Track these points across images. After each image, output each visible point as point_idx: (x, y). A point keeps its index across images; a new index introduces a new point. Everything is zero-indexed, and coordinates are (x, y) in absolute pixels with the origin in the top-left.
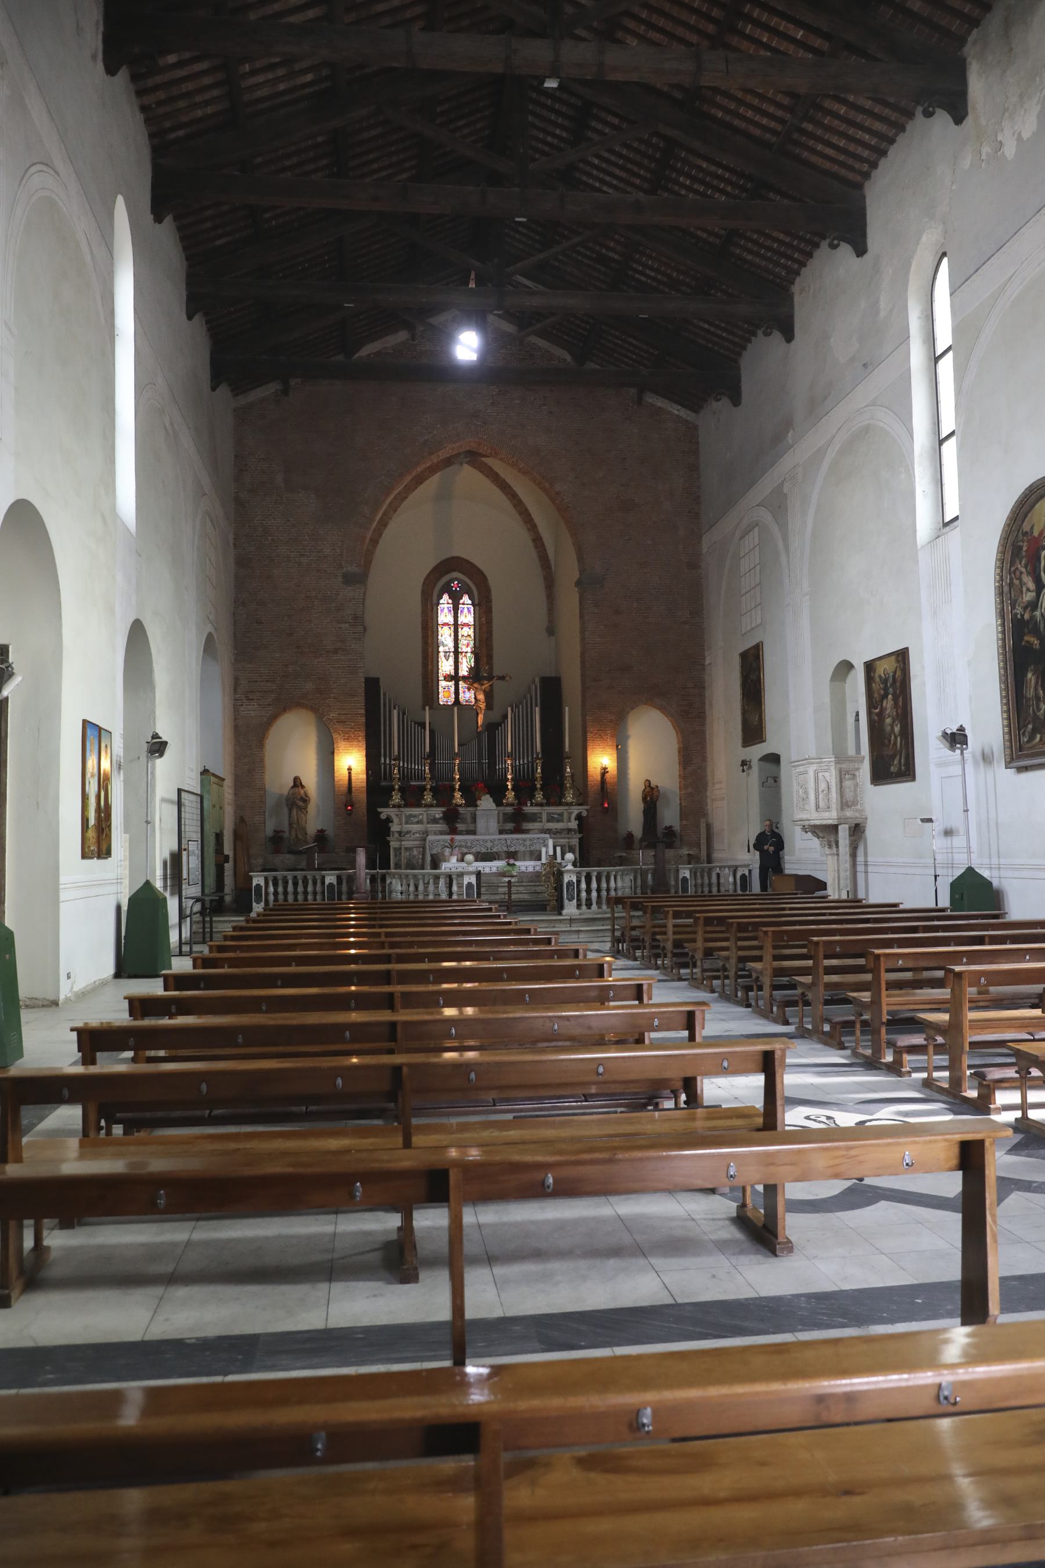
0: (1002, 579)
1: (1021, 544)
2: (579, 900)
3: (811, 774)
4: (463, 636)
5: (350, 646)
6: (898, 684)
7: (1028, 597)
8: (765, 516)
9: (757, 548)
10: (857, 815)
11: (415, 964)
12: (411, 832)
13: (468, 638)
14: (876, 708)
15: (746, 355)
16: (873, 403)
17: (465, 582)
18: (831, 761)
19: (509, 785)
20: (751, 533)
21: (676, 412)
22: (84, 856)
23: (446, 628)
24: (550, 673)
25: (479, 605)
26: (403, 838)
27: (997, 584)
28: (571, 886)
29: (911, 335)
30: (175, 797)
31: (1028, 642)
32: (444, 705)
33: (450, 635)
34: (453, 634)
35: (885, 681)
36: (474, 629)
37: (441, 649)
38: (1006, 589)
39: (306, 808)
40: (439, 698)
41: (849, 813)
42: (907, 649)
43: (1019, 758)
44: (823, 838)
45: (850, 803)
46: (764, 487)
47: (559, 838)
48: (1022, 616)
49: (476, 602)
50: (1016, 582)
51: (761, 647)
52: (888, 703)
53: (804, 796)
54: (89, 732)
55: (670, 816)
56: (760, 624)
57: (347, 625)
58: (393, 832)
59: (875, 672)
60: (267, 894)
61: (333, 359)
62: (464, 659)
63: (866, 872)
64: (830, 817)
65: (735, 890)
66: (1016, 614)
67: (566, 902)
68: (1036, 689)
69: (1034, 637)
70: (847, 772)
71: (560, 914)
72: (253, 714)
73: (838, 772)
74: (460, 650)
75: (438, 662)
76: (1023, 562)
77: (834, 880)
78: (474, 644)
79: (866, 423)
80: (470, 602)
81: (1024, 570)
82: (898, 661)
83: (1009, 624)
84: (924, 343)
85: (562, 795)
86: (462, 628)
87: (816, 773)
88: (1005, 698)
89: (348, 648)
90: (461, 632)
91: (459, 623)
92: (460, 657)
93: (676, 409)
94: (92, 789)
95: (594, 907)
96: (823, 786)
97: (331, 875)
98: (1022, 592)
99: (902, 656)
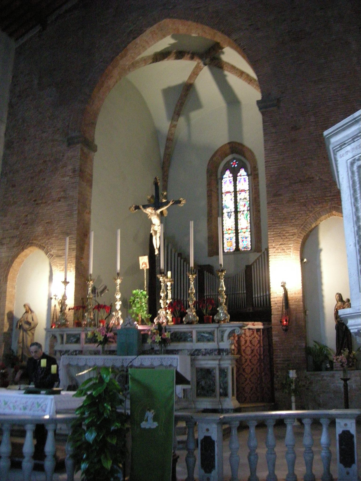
5: (69, 194)
13: (245, 200)
19: (223, 299)
23: (228, 195)
32: (227, 252)
33: (231, 200)
34: (233, 198)
37: (225, 211)
49: (250, 173)
53: (229, 239)
57: (68, 178)
62: (242, 216)
74: (238, 210)
78: (249, 204)
80: (245, 174)
85: (215, 312)
86: (240, 194)
89: (67, 196)
90: (239, 196)
91: (238, 190)
92: (239, 215)
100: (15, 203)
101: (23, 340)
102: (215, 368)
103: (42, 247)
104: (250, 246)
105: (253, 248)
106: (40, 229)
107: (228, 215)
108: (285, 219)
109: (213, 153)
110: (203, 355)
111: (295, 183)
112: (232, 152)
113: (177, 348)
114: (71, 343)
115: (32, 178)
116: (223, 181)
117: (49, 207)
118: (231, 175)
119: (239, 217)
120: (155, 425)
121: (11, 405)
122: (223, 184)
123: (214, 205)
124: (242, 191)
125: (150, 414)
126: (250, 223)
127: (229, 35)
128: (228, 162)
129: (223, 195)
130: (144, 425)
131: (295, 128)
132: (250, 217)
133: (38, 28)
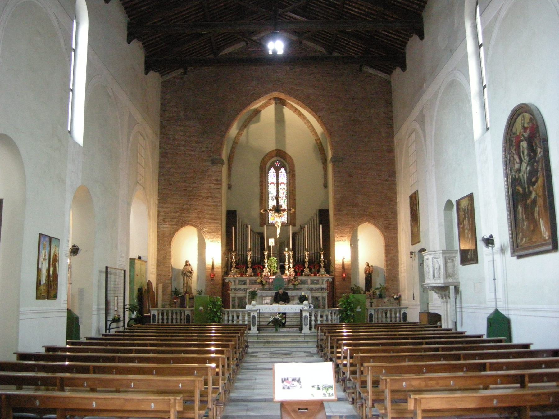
0: (506, 157)
1: (512, 139)
2: (310, 324)
3: (431, 260)
4: (281, 189)
5: (214, 195)
6: (469, 212)
7: (517, 166)
8: (417, 126)
9: (415, 143)
10: (455, 281)
11: (176, 355)
12: (240, 289)
13: (284, 190)
14: (461, 225)
15: (408, 46)
16: (455, 69)
17: (282, 162)
18: (440, 253)
19: (322, 265)
20: (412, 135)
21: (380, 75)
22: (38, 298)
23: (272, 185)
24: (323, 207)
25: (289, 173)
26: (237, 292)
27: (504, 160)
28: (306, 318)
29: (467, 35)
30: (104, 270)
31: (518, 190)
32: (271, 224)
33: (275, 188)
34: (276, 188)
35: (464, 211)
36: (287, 185)
37: (270, 196)
38: (508, 162)
39: (191, 276)
40: (268, 221)
41: (450, 280)
42: (472, 194)
43: (517, 251)
44: (439, 293)
45: (451, 275)
46: (416, 111)
47: (317, 293)
48: (515, 176)
49: (288, 172)
50: (512, 158)
51: (417, 193)
52: (466, 222)
54: (42, 240)
55: (378, 282)
56: (417, 181)
57: (213, 185)
58: (231, 289)
59: (460, 206)
60: (158, 319)
61: (208, 56)
62: (282, 200)
63: (462, 312)
64: (440, 282)
65: (400, 321)
66: (513, 175)
67: (304, 326)
68: (522, 215)
69: (520, 187)
70: (449, 258)
71: (301, 333)
72: (166, 229)
73: (444, 259)
74: (279, 196)
75: (268, 202)
76: (514, 148)
77: (444, 315)
78: (287, 193)
79: (452, 79)
80: (285, 172)
81: (514, 152)
82: (469, 200)
83: (510, 181)
84: (473, 39)
87: (433, 259)
88: (510, 219)
90: (280, 187)
91: (279, 182)
93: (380, 74)
94: (44, 266)
95: (313, 329)
96: (436, 266)
97: (154, 310)
98: (514, 163)
99: (471, 197)
100: (173, 196)
101: (187, 283)
102: (320, 297)
103: (195, 226)
104: (286, 221)
105: (289, 222)
106: (194, 215)
107: (272, 199)
108: (343, 223)
109: (264, 155)
110: (314, 290)
111: (349, 206)
112: (276, 156)
113: (300, 287)
114: (241, 284)
115: (185, 181)
116: (269, 175)
117: (200, 202)
118: (275, 171)
119: (279, 201)
120: (360, 310)
121: (294, 309)
122: (269, 177)
123: (264, 191)
124: (282, 183)
125: (359, 307)
126: (287, 206)
127: (316, 113)
128: (273, 162)
129: (269, 185)
130: (357, 310)
131: (350, 176)
132: (287, 202)
133: (181, 71)
